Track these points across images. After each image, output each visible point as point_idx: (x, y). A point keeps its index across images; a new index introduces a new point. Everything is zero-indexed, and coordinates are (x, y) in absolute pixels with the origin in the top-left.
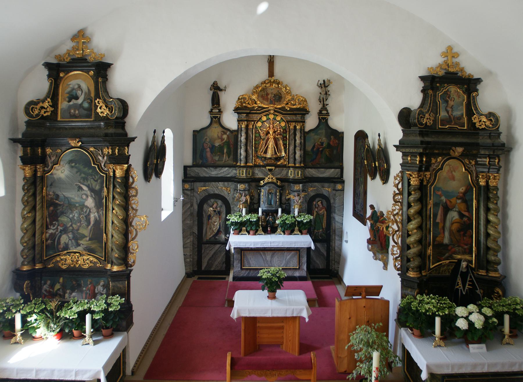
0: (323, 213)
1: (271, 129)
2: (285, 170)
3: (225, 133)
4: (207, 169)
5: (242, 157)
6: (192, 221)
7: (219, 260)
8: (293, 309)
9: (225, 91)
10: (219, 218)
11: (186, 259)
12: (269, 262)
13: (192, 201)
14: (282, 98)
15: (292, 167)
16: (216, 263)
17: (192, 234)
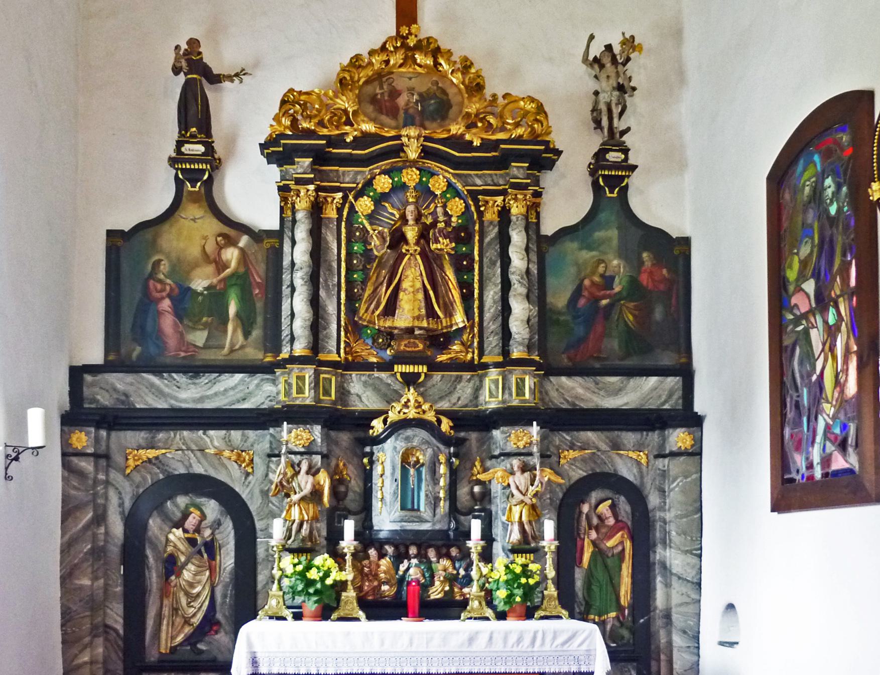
0: (620, 548)
2: (469, 380)
3: (231, 242)
4: (162, 377)
10: (212, 570)
13: (101, 501)
15: (497, 365)
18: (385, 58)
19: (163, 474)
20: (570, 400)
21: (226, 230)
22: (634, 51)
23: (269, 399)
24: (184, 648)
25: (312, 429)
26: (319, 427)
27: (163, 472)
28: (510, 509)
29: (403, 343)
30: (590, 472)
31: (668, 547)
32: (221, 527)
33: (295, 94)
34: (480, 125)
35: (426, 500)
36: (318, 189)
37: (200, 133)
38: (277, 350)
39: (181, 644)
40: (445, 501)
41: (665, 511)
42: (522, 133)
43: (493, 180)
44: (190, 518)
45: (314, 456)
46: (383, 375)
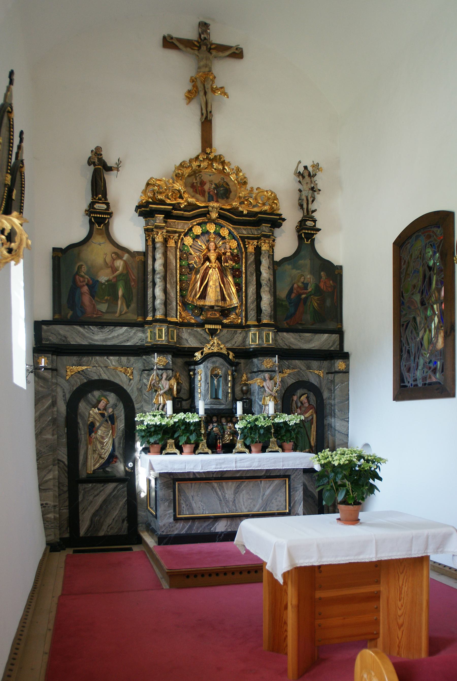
0: (311, 417)
1: (212, 251)
2: (240, 333)
3: (119, 257)
4: (84, 328)
5: (158, 302)
6: (56, 436)
7: (115, 513)
8: (427, 537)
9: (118, 170)
10: (112, 429)
11: (45, 514)
12: (231, 503)
14: (231, 192)
15: (255, 326)
16: (109, 521)
17: (56, 462)
18: (198, 164)
19: (86, 379)
20: (288, 344)
21: (116, 250)
22: (319, 171)
23: (141, 340)
24: (99, 470)
25: (167, 357)
26: (171, 356)
27: (86, 378)
28: (264, 398)
29: (209, 313)
30: (297, 381)
31: (333, 418)
32: (117, 408)
33: (154, 180)
34: (246, 202)
35: (223, 393)
36: (167, 232)
37: (103, 198)
38: (145, 315)
39: (98, 469)
40: (231, 394)
41: (331, 399)
42: (267, 209)
43: (251, 232)
44: (102, 403)
45: (168, 371)
46: (199, 329)
